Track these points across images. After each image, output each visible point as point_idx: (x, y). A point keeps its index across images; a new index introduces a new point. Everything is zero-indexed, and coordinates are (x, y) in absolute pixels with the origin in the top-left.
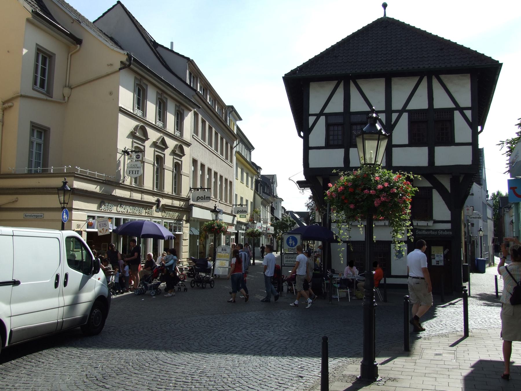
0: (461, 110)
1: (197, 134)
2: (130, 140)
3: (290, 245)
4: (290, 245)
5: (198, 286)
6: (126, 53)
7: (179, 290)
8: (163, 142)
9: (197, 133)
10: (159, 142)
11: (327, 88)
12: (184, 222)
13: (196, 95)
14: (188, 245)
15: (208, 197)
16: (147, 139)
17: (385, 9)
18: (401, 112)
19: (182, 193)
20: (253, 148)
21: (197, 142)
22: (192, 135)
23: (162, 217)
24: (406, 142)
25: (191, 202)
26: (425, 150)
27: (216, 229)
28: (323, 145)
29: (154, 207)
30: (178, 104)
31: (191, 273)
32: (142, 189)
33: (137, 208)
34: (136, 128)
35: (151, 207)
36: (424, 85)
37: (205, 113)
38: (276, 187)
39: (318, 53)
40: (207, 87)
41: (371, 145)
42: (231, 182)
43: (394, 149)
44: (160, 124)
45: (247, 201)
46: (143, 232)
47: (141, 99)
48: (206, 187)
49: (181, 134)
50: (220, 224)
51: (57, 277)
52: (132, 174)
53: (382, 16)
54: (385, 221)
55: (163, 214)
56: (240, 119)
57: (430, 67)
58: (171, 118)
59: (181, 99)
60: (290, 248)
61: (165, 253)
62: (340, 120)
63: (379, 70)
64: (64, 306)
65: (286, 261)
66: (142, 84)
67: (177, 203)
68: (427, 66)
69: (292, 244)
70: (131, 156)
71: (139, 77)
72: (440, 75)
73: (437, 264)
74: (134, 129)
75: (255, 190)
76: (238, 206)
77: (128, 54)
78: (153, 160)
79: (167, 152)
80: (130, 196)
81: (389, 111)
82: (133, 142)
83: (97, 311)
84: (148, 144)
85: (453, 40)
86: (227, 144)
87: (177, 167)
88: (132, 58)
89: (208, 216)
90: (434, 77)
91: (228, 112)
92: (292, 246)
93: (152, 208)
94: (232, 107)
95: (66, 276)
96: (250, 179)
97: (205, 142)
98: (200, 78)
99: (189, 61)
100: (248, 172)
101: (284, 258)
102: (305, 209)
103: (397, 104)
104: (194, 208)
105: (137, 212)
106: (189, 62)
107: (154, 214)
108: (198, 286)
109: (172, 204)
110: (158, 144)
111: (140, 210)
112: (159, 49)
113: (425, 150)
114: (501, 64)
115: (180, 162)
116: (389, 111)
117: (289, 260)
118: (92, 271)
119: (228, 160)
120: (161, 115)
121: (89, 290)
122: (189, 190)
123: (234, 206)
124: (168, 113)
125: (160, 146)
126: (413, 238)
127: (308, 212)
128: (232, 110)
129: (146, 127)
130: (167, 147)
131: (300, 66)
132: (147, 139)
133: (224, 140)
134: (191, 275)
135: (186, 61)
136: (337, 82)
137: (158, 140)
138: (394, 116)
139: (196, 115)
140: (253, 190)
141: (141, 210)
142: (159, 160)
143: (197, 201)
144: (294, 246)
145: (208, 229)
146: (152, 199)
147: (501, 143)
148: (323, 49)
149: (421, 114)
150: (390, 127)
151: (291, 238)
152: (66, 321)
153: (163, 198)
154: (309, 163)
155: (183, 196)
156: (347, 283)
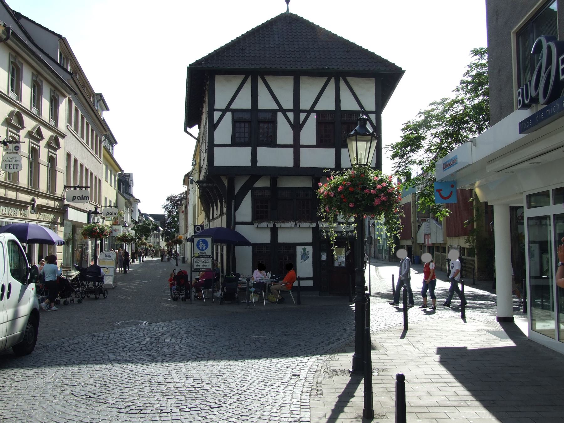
0: (284, 112)
1: (71, 125)
2: (5, 128)
3: (201, 248)
4: (201, 248)
5: (88, 297)
6: (2, 24)
7: (72, 302)
8: (39, 132)
9: (71, 124)
10: (35, 131)
11: (233, 83)
12: (59, 225)
13: (72, 80)
14: (63, 252)
15: (86, 197)
16: (23, 127)
17: (288, 4)
18: (309, 112)
19: (57, 192)
20: (116, 143)
21: (71, 133)
22: (66, 126)
23: (36, 219)
24: (314, 143)
25: (66, 202)
26: (332, 151)
27: (98, 233)
28: (230, 143)
29: (29, 208)
30: (53, 89)
31: (75, 283)
32: (17, 186)
33: (12, 208)
34: (11, 114)
35: (26, 208)
36: (332, 84)
37: (78, 101)
38: (132, 186)
39: (223, 44)
40: (77, 70)
41: (362, 146)
42: (100, 180)
43: (216, 149)
44: (35, 111)
45: (110, 202)
46: (29, 237)
47: (15, 79)
48: (72, 185)
49: (55, 123)
50: (102, 228)
51: (3, 286)
52: (10, 168)
53: (285, 11)
54: (291, 223)
55: (38, 215)
56: (107, 109)
57: (338, 68)
58: (46, 104)
59: (57, 83)
60: (200, 251)
61: (44, 261)
62: (247, 116)
63: (289, 67)
64: (7, 322)
65: (196, 266)
66: (17, 62)
67: (52, 203)
68: (336, 68)
69: (202, 247)
70: (8, 148)
71: (14, 54)
72: (347, 78)
73: (339, 265)
74: (9, 115)
75: (118, 190)
76: (108, 207)
77: (4, 26)
78: (27, 153)
79: (43, 143)
80: (5, 195)
81: (297, 110)
82: (8, 130)
83: (31, 326)
84: (23, 133)
85: (358, 43)
86: (96, 136)
87: (52, 161)
88: (11, 31)
89: (82, 218)
90: (341, 79)
91: (96, 101)
92: (203, 250)
93: (27, 209)
94: (101, 95)
95: (10, 285)
96: (113, 177)
97: (78, 133)
98: (70, 60)
99: (61, 39)
100: (112, 169)
101: (194, 262)
102: (162, 212)
103: (305, 104)
104: (70, 210)
105: (12, 214)
106: (61, 40)
107: (29, 216)
108: (88, 297)
109: (47, 204)
110: (34, 134)
111: (15, 211)
112: (22, 21)
113: (332, 151)
114: (404, 72)
115: (55, 156)
116: (297, 110)
117: (199, 264)
118: (27, 281)
119: (97, 155)
120: (36, 101)
121: (25, 303)
122: (63, 188)
123: (103, 208)
124: (43, 99)
125: (35, 136)
126: (400, 236)
127: (164, 215)
128: (100, 98)
129: (23, 115)
130: (42, 138)
131: (205, 57)
132: (23, 127)
133: (94, 132)
134: (74, 286)
135: (57, 38)
136: (326, 79)
137: (34, 129)
138: (303, 116)
139: (70, 102)
140: (115, 190)
141: (16, 211)
142: (34, 152)
143: (73, 201)
144: (204, 250)
145: (88, 232)
146: (24, 197)
147: (387, 146)
148: (228, 41)
149: (328, 115)
150: (297, 127)
151: (201, 241)
152: (10, 338)
153: (38, 197)
154: (215, 161)
155: (57, 196)
156: (260, 286)
